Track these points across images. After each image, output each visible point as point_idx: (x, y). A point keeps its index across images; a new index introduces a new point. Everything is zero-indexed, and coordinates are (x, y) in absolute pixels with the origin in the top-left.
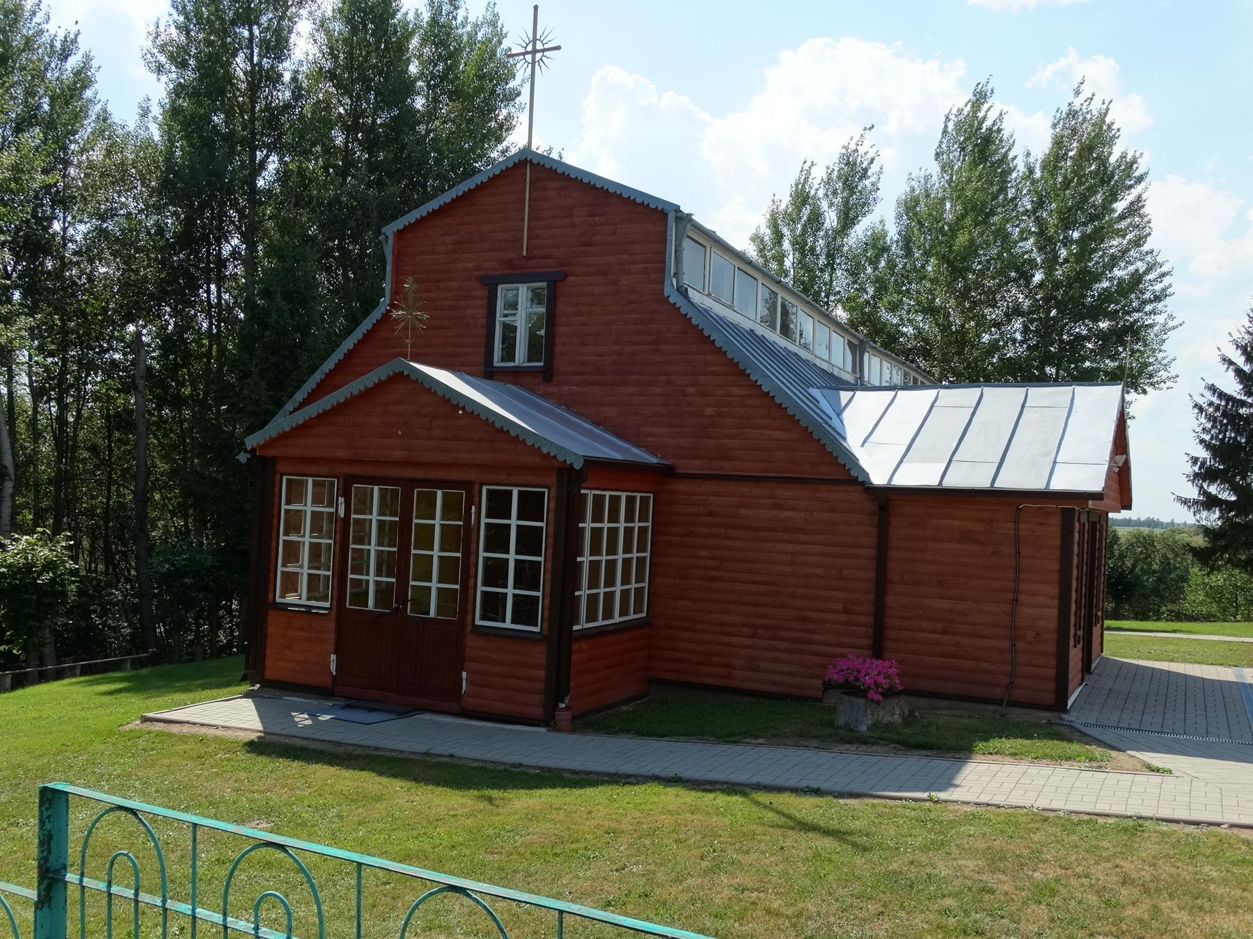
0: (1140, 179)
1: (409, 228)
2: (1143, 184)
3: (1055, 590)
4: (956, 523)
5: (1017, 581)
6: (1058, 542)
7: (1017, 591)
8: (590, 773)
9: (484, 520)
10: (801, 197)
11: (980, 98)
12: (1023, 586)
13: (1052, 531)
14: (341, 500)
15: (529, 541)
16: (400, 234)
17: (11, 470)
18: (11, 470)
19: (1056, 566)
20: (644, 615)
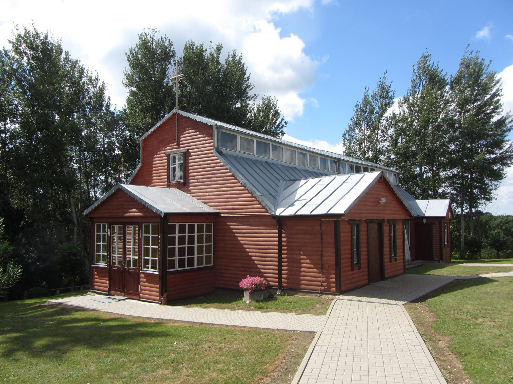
0: (498, 82)
1: (145, 139)
2: (499, 84)
3: (333, 250)
4: (302, 228)
5: (322, 247)
6: (333, 233)
7: (322, 251)
8: (264, 329)
9: (143, 235)
10: (366, 102)
11: (425, 58)
12: (324, 249)
13: (331, 229)
14: (109, 230)
15: (208, 239)
16: (144, 141)
17: (76, 223)
18: (76, 223)
19: (333, 241)
20: (212, 265)
